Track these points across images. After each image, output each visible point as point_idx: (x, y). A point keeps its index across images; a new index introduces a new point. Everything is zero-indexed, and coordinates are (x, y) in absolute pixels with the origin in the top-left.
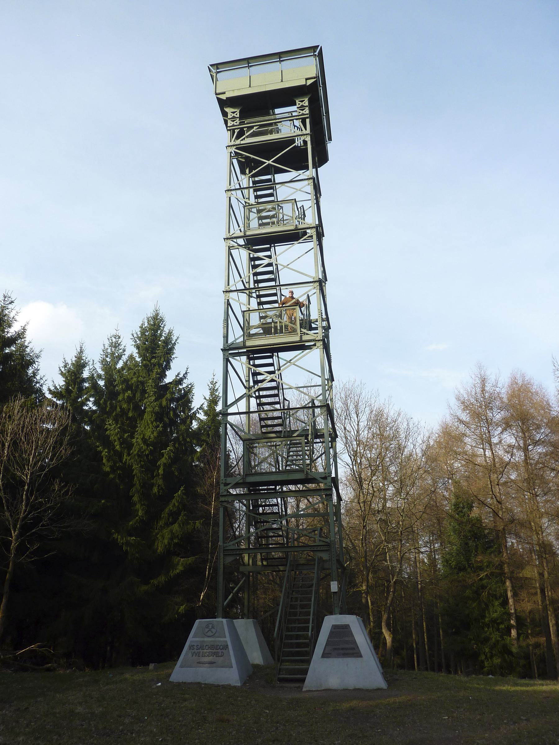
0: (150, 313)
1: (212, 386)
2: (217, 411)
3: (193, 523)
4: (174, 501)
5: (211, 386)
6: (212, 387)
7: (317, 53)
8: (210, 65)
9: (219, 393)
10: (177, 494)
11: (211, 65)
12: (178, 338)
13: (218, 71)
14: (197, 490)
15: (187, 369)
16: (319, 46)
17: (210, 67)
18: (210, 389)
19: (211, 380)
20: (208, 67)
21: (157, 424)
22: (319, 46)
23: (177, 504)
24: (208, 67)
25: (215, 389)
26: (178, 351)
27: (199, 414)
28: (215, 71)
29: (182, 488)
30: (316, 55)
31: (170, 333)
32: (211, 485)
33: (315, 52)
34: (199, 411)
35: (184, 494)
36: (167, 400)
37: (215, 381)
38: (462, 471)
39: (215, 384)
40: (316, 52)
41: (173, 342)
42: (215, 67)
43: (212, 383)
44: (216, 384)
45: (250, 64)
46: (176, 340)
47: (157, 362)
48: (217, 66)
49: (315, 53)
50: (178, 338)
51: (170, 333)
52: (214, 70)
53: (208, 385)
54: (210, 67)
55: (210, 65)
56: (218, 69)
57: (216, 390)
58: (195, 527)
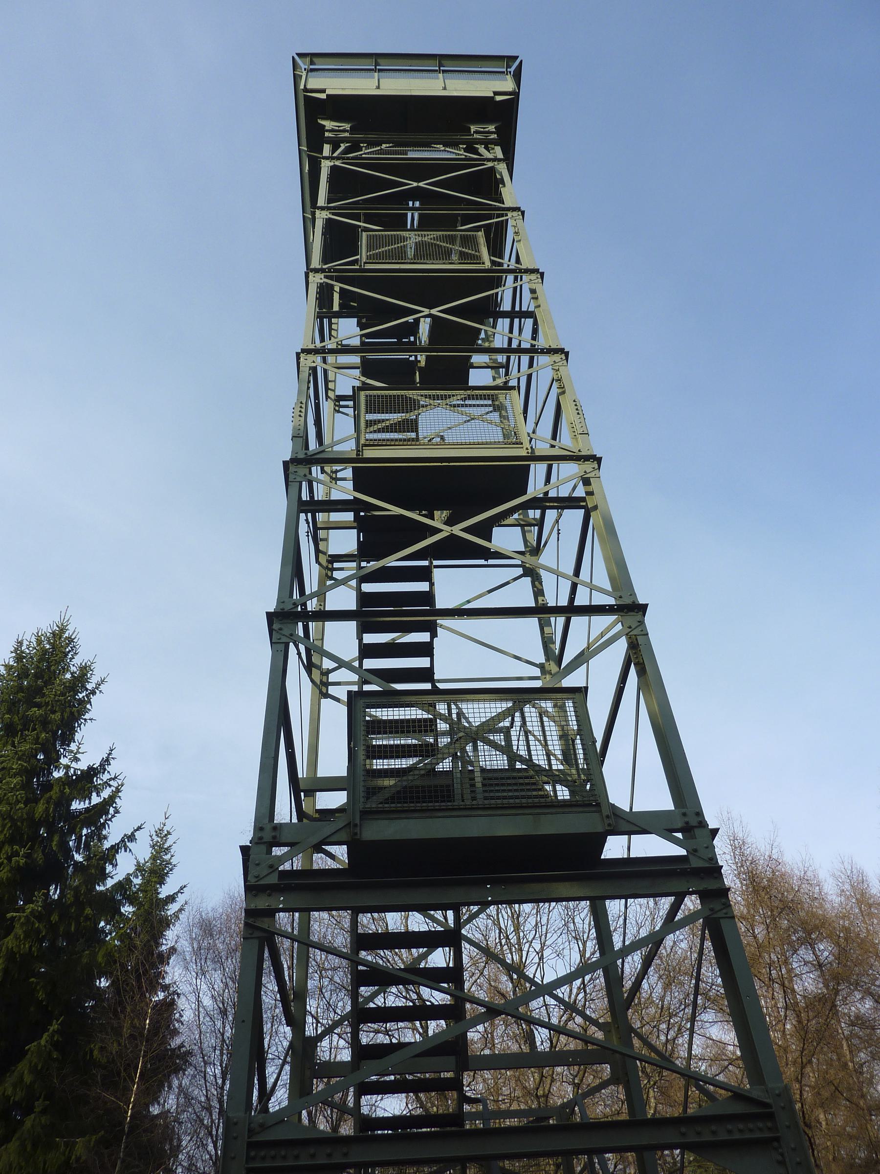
0: (46, 624)
1: (159, 840)
2: (161, 896)
3: (67, 1145)
4: (23, 1067)
5: (156, 839)
6: (158, 842)
7: (512, 69)
8: (297, 54)
9: (172, 856)
10: (35, 1043)
11: (299, 55)
12: (103, 681)
13: (312, 67)
14: (92, 1051)
15: (112, 750)
16: (517, 57)
17: (296, 57)
18: (153, 847)
19: (158, 826)
20: (293, 57)
21: (13, 849)
22: (517, 57)
23: (28, 1079)
24: (293, 57)
25: (165, 847)
26: (98, 706)
27: (126, 851)
28: (307, 67)
29: (55, 1026)
30: (510, 72)
31: (85, 670)
32: (136, 1035)
33: (508, 66)
34: (128, 844)
35: (55, 1045)
36: (48, 802)
37: (165, 829)
38: (810, 957)
39: (166, 835)
40: (510, 68)
41: (90, 686)
42: (308, 59)
43: (159, 832)
44: (169, 836)
45: (379, 65)
46: (98, 685)
47: (41, 715)
48: (313, 57)
49: (508, 70)
50: (103, 681)
51: (85, 670)
52: (305, 64)
53: (151, 837)
54: (296, 57)
55: (297, 54)
56: (312, 63)
57: (167, 849)
58: (70, 1158)
